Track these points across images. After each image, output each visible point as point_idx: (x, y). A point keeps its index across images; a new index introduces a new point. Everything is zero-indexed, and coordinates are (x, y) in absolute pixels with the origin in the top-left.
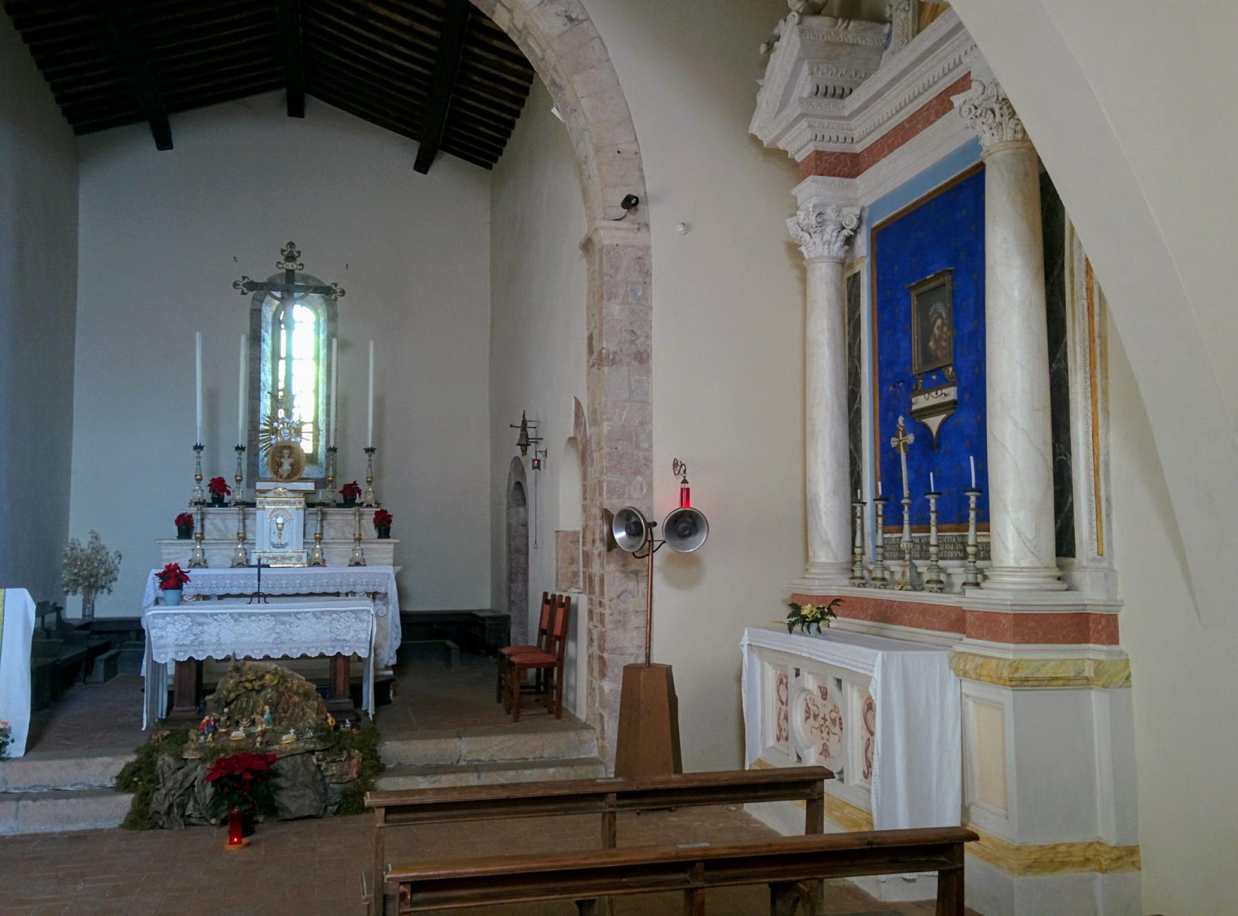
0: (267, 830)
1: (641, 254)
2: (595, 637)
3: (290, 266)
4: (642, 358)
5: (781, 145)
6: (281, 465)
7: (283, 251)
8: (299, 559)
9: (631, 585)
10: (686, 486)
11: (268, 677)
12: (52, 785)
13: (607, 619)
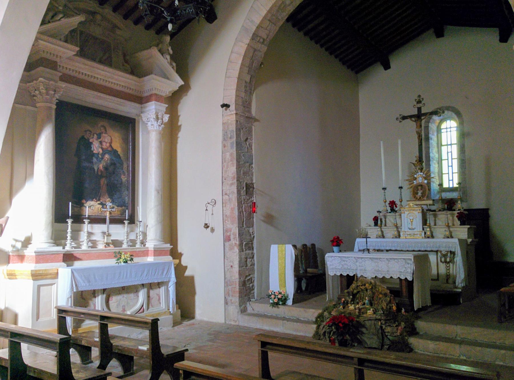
3: (419, 106)
6: (417, 193)
11: (367, 285)
12: (297, 317)
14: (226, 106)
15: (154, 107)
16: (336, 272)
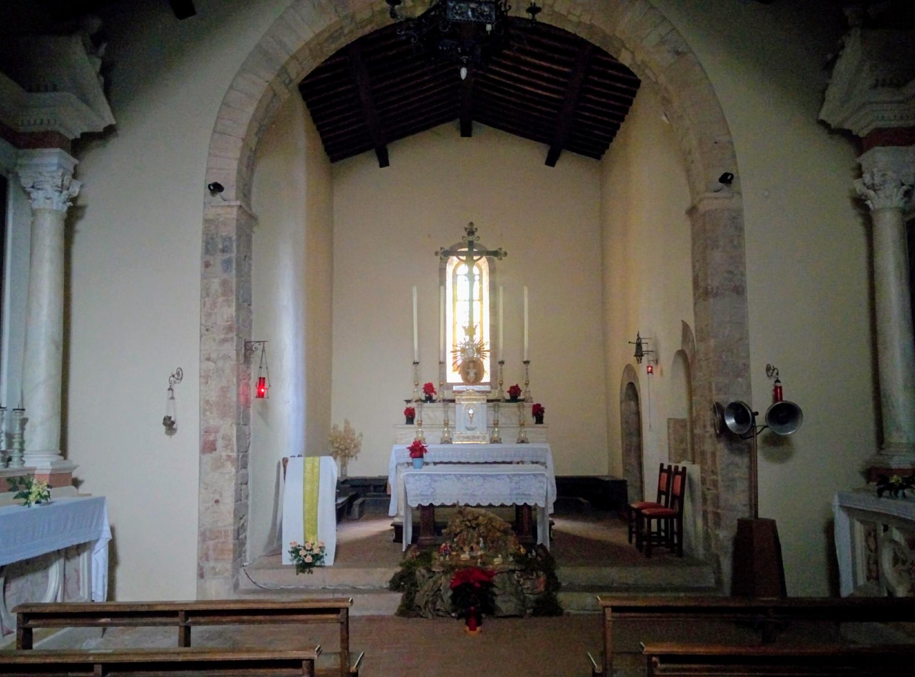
0: (489, 624)
1: (734, 215)
2: (709, 497)
4: (739, 291)
5: (846, 126)
6: (468, 373)
7: (466, 229)
8: (484, 438)
9: (737, 459)
10: (778, 384)
11: (481, 518)
13: (720, 483)
14: (216, 188)
15: (55, 160)
16: (422, 500)
